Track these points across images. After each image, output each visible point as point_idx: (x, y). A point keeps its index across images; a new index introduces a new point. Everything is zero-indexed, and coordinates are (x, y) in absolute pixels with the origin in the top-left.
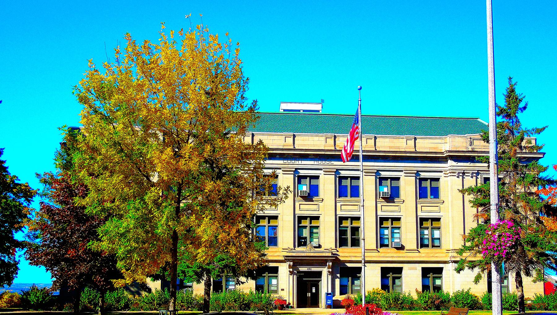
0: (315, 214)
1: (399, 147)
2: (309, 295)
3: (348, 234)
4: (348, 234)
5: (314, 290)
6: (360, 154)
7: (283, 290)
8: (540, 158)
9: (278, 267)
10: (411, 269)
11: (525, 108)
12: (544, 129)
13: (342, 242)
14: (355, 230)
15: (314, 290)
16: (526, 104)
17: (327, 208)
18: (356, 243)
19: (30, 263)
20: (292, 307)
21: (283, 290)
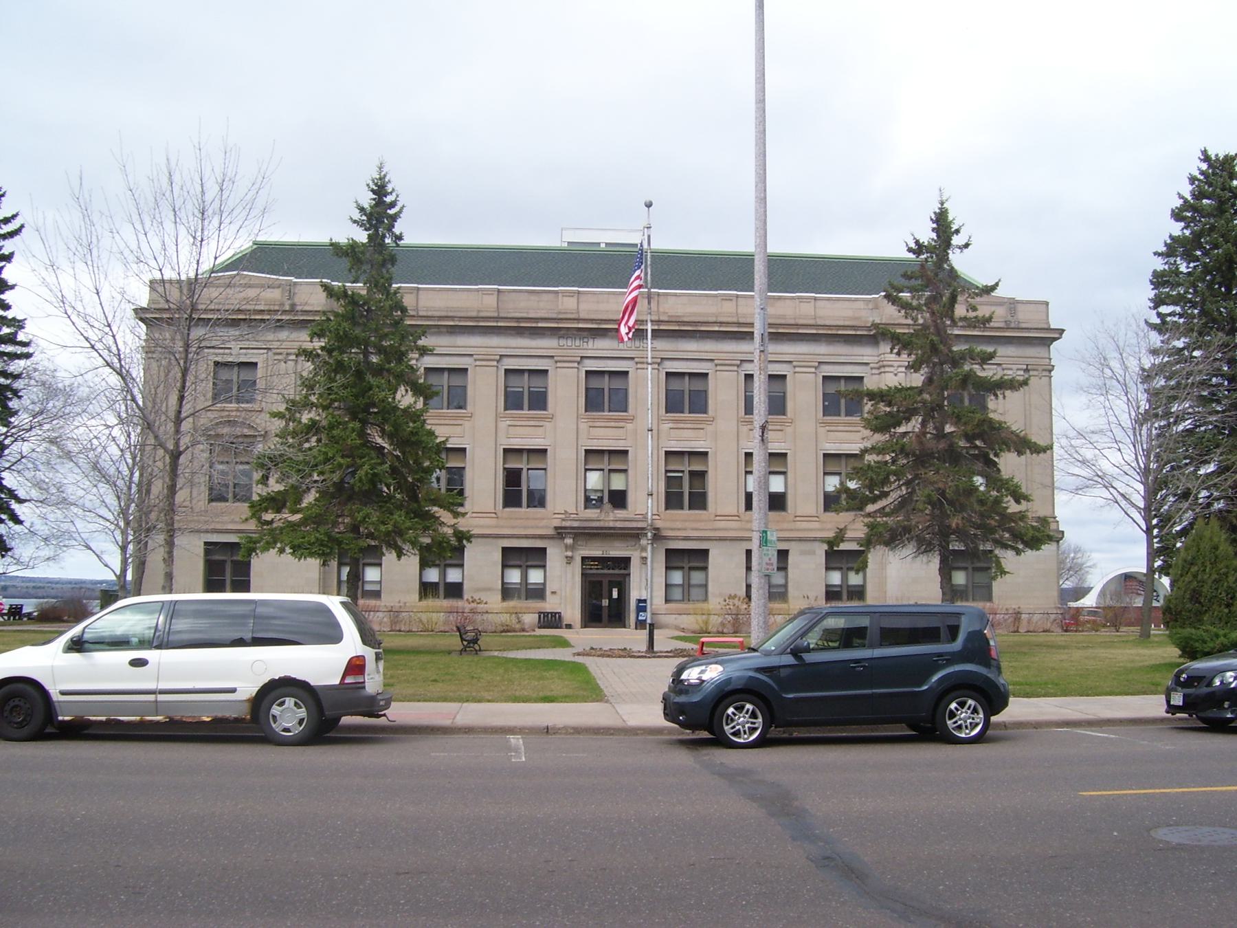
0: (619, 445)
1: (784, 317)
2: (605, 602)
3: (687, 485)
4: (687, 485)
5: (615, 595)
6: (649, 327)
7: (553, 593)
8: (1055, 339)
9: (544, 550)
10: (803, 553)
11: (967, 246)
12: (997, 284)
13: (673, 500)
14: (699, 477)
15: (615, 595)
16: (22, 226)
17: (647, 434)
18: (699, 501)
19: (1018, 497)
20: (569, 626)
21: (553, 593)
